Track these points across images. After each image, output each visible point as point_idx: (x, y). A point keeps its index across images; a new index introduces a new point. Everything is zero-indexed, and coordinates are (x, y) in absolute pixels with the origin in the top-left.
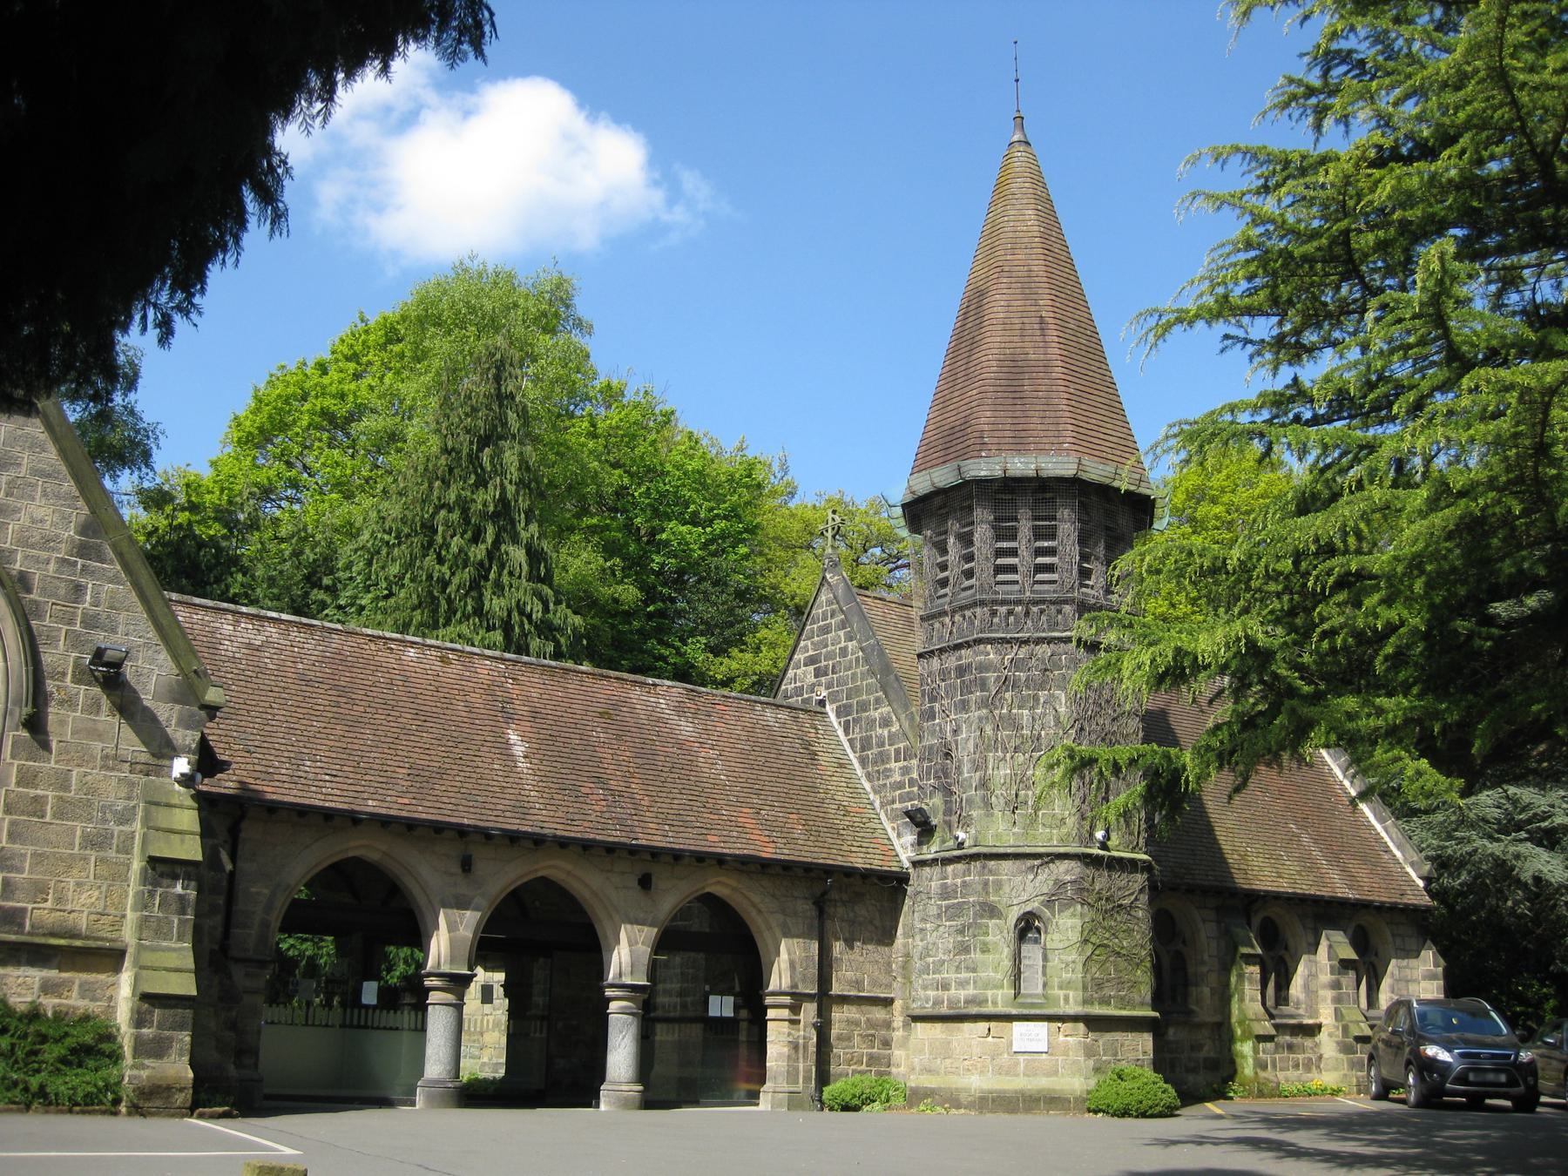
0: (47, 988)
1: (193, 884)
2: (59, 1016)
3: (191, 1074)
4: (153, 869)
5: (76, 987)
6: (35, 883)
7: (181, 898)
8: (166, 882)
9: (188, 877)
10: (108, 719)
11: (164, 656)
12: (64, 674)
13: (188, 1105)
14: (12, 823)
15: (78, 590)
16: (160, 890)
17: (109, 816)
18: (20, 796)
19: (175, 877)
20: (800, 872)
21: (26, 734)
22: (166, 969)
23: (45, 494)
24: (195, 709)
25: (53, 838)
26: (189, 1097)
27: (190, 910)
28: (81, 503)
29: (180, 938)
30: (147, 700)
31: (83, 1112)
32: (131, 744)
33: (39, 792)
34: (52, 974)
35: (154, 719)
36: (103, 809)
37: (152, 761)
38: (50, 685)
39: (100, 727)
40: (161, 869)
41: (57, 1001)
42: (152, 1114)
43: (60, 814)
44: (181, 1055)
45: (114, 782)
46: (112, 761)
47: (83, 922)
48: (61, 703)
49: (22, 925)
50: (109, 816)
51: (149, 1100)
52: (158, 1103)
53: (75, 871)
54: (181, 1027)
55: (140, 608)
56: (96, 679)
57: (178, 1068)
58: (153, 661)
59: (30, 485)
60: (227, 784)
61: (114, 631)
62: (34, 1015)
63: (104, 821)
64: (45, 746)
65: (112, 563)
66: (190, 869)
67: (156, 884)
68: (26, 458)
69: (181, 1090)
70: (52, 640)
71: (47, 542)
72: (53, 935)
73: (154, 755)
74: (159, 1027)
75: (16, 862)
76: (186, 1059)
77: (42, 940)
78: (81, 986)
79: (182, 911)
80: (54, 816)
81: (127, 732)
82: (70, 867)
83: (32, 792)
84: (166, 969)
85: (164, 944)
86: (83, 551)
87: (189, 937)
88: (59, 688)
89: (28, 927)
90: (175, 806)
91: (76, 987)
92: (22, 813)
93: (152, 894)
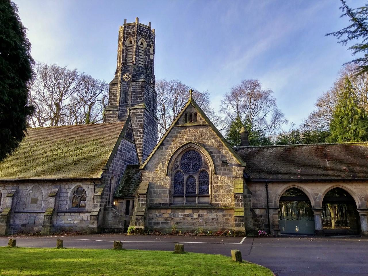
12: (219, 165)
16: (237, 198)
33: (218, 185)
40: (237, 195)
87: (243, 206)
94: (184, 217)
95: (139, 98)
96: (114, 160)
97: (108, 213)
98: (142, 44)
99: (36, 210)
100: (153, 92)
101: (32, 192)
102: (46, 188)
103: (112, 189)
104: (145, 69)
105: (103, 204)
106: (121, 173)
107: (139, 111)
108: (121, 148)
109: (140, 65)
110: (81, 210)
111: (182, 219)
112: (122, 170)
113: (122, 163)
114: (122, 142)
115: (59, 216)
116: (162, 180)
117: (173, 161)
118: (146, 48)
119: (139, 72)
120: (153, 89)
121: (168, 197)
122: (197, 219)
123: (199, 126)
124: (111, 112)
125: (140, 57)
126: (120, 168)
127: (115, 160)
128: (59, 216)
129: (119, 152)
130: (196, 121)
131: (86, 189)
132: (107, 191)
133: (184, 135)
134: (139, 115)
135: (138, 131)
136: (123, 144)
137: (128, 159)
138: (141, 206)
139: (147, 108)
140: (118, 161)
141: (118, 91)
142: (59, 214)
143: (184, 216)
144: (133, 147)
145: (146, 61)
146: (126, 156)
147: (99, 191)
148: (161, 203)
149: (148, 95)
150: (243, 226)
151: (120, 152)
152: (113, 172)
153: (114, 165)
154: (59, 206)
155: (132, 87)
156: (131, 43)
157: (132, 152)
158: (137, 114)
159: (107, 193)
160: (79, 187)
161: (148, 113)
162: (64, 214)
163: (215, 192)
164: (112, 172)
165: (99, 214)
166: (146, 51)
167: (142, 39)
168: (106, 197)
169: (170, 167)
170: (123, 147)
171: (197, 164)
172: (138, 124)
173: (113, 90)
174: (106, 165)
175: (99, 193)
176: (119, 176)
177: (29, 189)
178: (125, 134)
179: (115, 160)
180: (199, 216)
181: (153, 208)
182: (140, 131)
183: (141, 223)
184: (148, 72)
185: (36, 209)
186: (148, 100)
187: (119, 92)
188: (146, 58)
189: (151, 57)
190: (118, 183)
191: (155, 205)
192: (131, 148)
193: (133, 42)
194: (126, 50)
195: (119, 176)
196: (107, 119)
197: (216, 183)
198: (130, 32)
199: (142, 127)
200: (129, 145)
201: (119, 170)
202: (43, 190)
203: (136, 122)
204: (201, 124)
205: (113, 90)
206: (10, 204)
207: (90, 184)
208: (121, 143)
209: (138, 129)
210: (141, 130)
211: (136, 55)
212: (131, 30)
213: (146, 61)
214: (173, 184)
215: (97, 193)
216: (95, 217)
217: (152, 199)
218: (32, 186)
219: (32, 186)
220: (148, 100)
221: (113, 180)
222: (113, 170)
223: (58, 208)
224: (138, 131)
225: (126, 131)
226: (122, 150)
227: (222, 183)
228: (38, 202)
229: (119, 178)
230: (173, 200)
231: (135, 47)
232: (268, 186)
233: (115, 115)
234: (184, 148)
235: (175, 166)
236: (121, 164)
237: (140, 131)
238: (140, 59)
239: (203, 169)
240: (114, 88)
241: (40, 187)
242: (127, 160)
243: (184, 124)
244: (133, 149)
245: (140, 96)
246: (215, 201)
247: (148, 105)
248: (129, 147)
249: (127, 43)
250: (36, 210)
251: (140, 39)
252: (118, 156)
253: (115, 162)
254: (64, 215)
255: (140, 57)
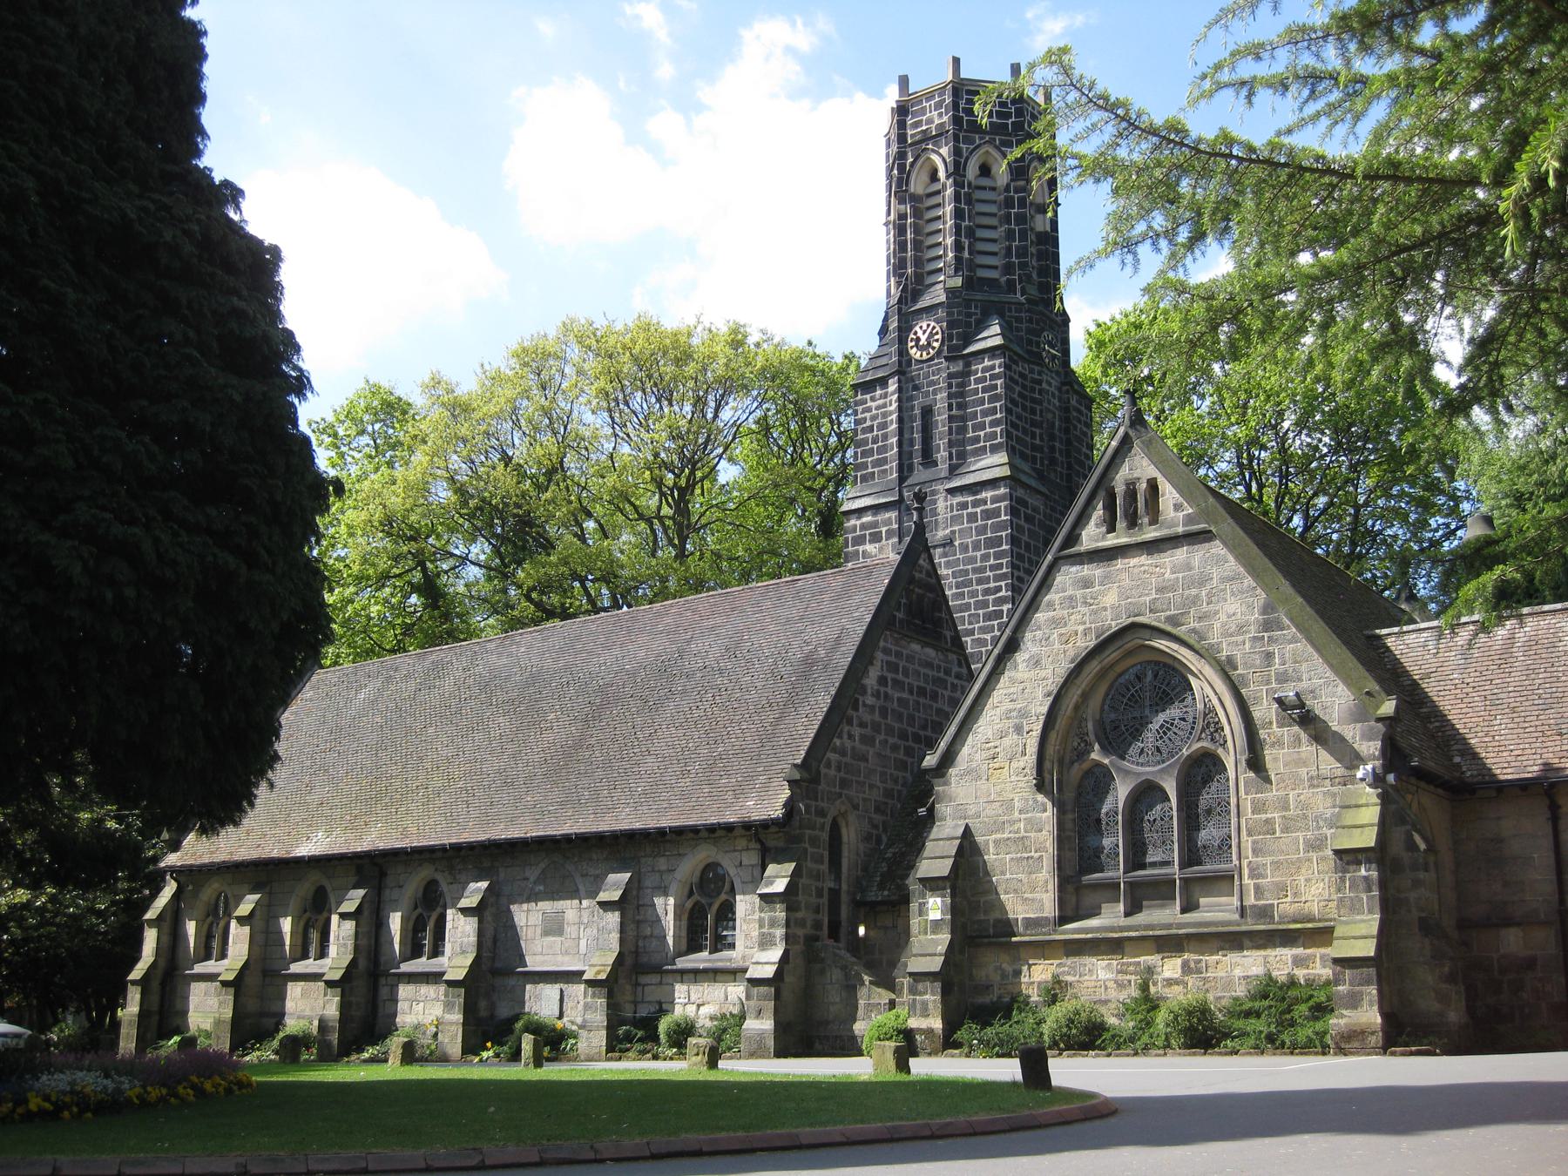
0: (1298, 962)
1: (1374, 866)
2: (1310, 983)
3: (1379, 1020)
4: (1341, 859)
5: (1318, 959)
6: (1276, 884)
7: (1366, 878)
8: (1352, 868)
9: (1369, 861)
10: (1308, 749)
11: (1341, 689)
12: (1271, 723)
13: (1380, 1045)
14: (1254, 842)
15: (1269, 656)
16: (1348, 875)
17: (1321, 823)
18: (1256, 821)
19: (1359, 863)
20: (704, 834)
21: (1252, 774)
22: (1355, 938)
23: (1233, 594)
24: (1373, 723)
25: (1284, 847)
26: (1380, 1039)
27: (1374, 888)
28: (1259, 591)
29: (1370, 911)
30: (1335, 726)
31: (1302, 1054)
32: (1328, 763)
33: (1269, 816)
34: (1299, 951)
35: (1343, 739)
36: (1316, 819)
37: (1346, 772)
38: (1263, 734)
39: (1303, 756)
40: (1348, 858)
41: (1306, 971)
42: (1352, 1054)
43: (1286, 830)
44: (1371, 1005)
45: (1321, 796)
46: (1315, 781)
47: (1315, 908)
48: (1273, 745)
49: (1272, 917)
50: (1321, 823)
51: (1349, 1042)
52: (1356, 1044)
53: (1303, 871)
54: (1368, 983)
55: (1316, 656)
56: (1294, 720)
57: (1370, 1016)
58: (1333, 694)
59: (1222, 590)
60: (1530, 769)
61: (1300, 680)
62: (1292, 983)
63: (1319, 828)
64: (1268, 780)
65: (1289, 628)
66: (1369, 854)
67: (1345, 871)
68: (1216, 573)
69: (1373, 1033)
70: (1258, 700)
71: (1241, 629)
72: (1295, 921)
73: (1347, 768)
74: (1351, 984)
75: (1261, 871)
76: (1376, 1008)
77: (1284, 927)
78: (1321, 958)
79: (1369, 890)
80: (1282, 832)
81: (1324, 754)
82: (1299, 868)
83: (1264, 816)
84: (1355, 938)
85: (1358, 917)
86: (1267, 626)
87: (1377, 909)
88: (1269, 735)
89: (1276, 918)
90: (1362, 806)
91: (1318, 959)
92: (1259, 834)
93: (1343, 880)
94: (1120, 977)
95: (982, 433)
96: (845, 736)
97: (822, 972)
98: (985, 170)
99: (562, 964)
100: (1065, 388)
101: (541, 888)
102: (592, 871)
103: (849, 870)
104: (1011, 284)
105: (800, 932)
106: (888, 793)
107: (987, 494)
108: (882, 680)
109: (982, 273)
110: (721, 960)
111: (1111, 984)
112: (896, 781)
113: (895, 748)
114: (886, 651)
115: (644, 986)
116: (1020, 812)
117: (1061, 723)
118: (1007, 189)
119: (976, 307)
120: (1057, 373)
121: (1050, 887)
122: (1176, 982)
123: (1173, 541)
124: (867, 519)
125: (981, 233)
126: (883, 774)
127: (850, 736)
128: (644, 986)
129: (870, 700)
130: (1154, 521)
131: (732, 871)
132: (818, 876)
133: (1103, 593)
134: (988, 515)
135: (987, 592)
136: (893, 659)
137: (924, 727)
138: (933, 932)
139: (1024, 478)
140: (865, 740)
141: (891, 413)
142: (644, 979)
143: (1119, 972)
144: (955, 669)
145: (1009, 249)
146: (911, 718)
147: (777, 877)
148: (1020, 917)
149: (1033, 412)
150: (1371, 1005)
151: (877, 695)
152: (845, 792)
153: (848, 759)
154: (641, 944)
155: (950, 386)
156: (934, 176)
157: (947, 693)
158: (978, 510)
159: (820, 884)
160: (711, 867)
161: (1034, 501)
162: (659, 976)
163: (1256, 852)
164: (838, 790)
165: (779, 973)
166: (1009, 203)
167: (986, 148)
168: (813, 900)
169: (1050, 751)
170: (890, 676)
171: (1172, 724)
172: (985, 557)
173: (869, 410)
174: (805, 759)
175: (780, 886)
176: (878, 810)
177: (532, 879)
178: (900, 615)
179: (850, 736)
180: (1186, 968)
181: (986, 940)
182: (999, 589)
183: (931, 1006)
184: (1022, 299)
185: (560, 958)
186: (1033, 436)
187: (894, 417)
188: (1010, 235)
189: (1041, 224)
190: (879, 841)
191: (994, 926)
192: (942, 675)
193: (942, 174)
194: (917, 213)
195: (878, 810)
196: (850, 549)
197: (1258, 808)
198: (924, 128)
199: (1004, 570)
200: (929, 665)
201: (876, 780)
202: (578, 879)
203: (976, 547)
204: (1180, 530)
205: (869, 410)
206: (473, 939)
207: (748, 849)
208: (879, 655)
209: (987, 580)
210: (1003, 584)
211: (958, 227)
212: (930, 121)
213: (1009, 249)
214: (1069, 825)
215: (772, 883)
216: (763, 989)
217: (982, 900)
218: (542, 865)
219: (542, 865)
220: (1033, 436)
221: (847, 825)
222: (844, 783)
223: (637, 953)
224: (987, 592)
225: (904, 601)
226: (889, 690)
227: (1286, 808)
228: (567, 929)
229: (878, 818)
230: (1074, 899)
231: (949, 191)
232: (1559, 807)
233: (884, 530)
234: (1112, 655)
235: (1076, 744)
236: (888, 752)
237: (999, 589)
238: (981, 246)
239: (1199, 745)
240: (873, 399)
241: (570, 867)
242: (922, 733)
243: (1104, 538)
244: (955, 681)
245: (988, 419)
246: (1256, 893)
247: (1034, 459)
248: (930, 673)
249: (918, 185)
250: (562, 964)
251: (971, 153)
252: (867, 718)
253: (848, 744)
254: (661, 983)
255: (981, 233)
